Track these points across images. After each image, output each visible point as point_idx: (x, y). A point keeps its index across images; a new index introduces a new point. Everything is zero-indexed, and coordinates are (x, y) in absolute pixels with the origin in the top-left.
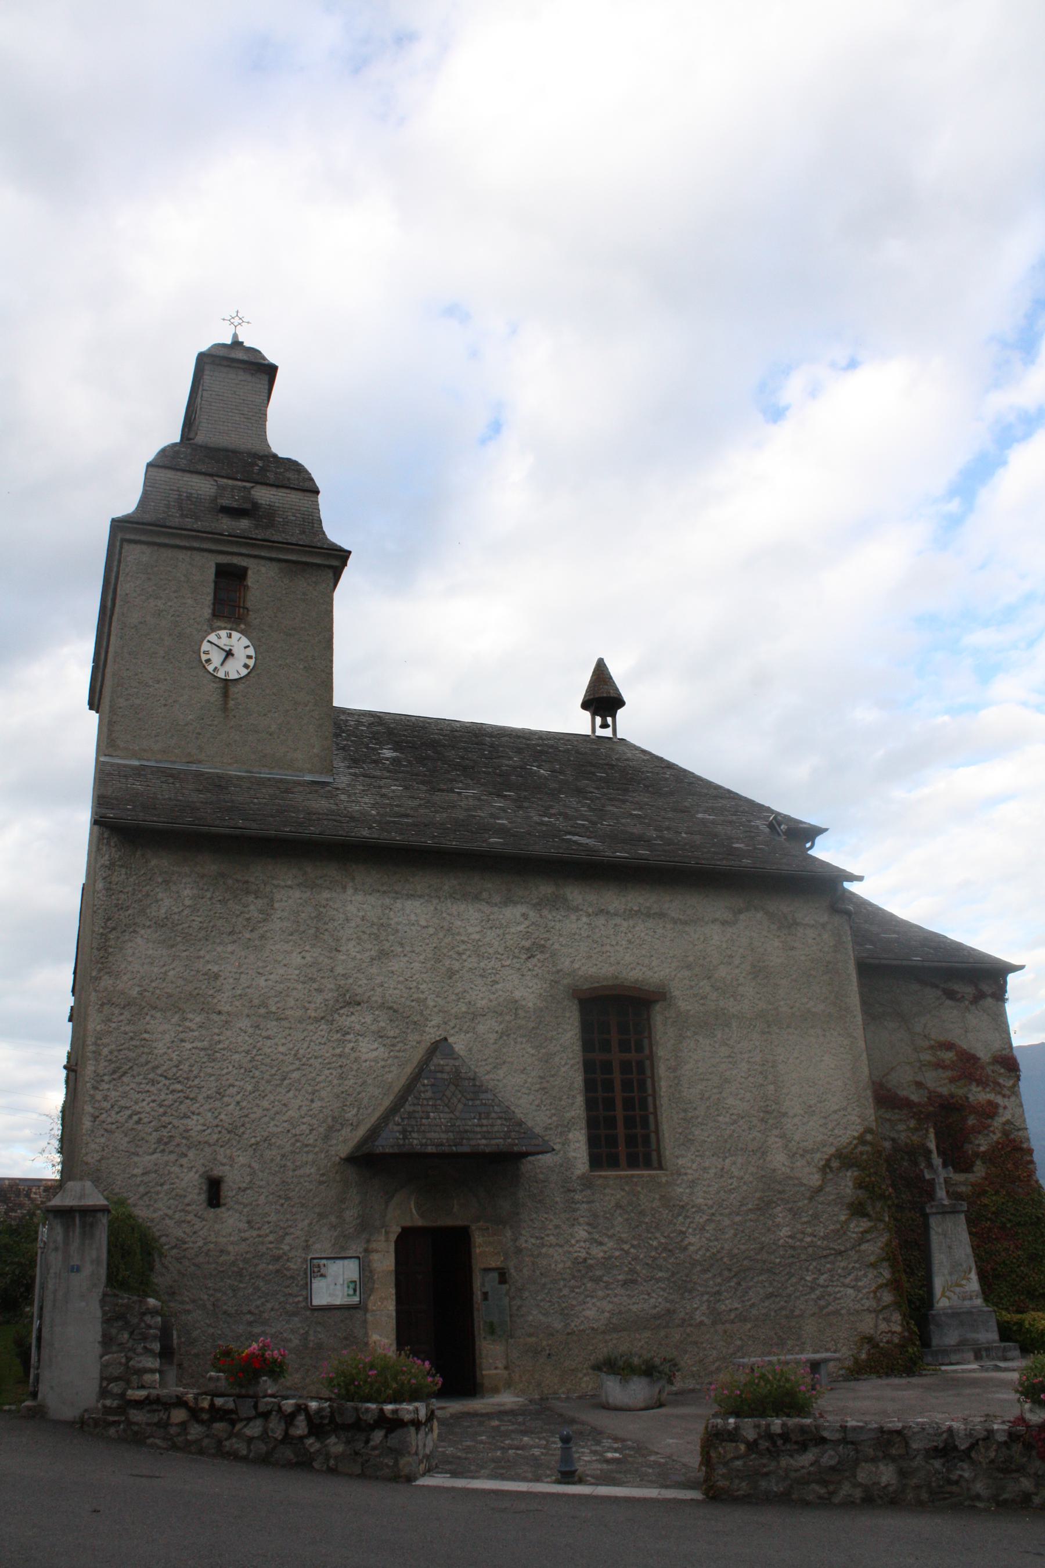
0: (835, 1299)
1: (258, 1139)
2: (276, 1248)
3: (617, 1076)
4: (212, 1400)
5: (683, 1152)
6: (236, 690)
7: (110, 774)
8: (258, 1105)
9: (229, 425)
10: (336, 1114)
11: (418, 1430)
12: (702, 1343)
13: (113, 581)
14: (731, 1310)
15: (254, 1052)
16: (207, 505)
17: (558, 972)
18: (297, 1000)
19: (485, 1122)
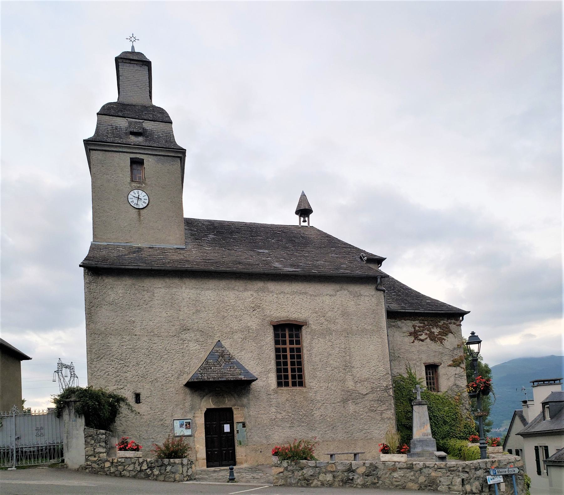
1: (153, 379)
3: (288, 354)
10: (182, 370)
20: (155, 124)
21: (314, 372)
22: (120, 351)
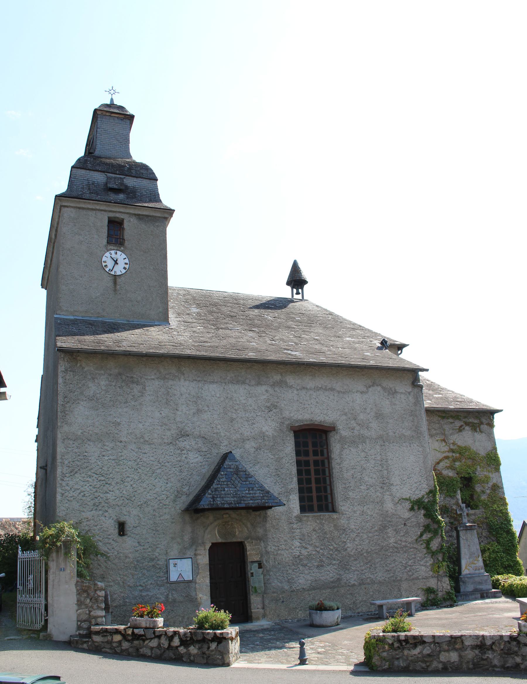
0: (416, 571)
1: (142, 502)
2: (152, 555)
3: (312, 468)
4: (133, 630)
5: (345, 504)
6: (120, 280)
7: (60, 324)
8: (141, 486)
9: (111, 146)
10: (179, 490)
11: (232, 641)
12: (354, 594)
13: (56, 225)
14: (368, 578)
15: (139, 460)
16: (102, 187)
17: (283, 418)
18: (159, 434)
19: (251, 492)
20: (138, 181)
21: (346, 492)
22: (99, 463)
